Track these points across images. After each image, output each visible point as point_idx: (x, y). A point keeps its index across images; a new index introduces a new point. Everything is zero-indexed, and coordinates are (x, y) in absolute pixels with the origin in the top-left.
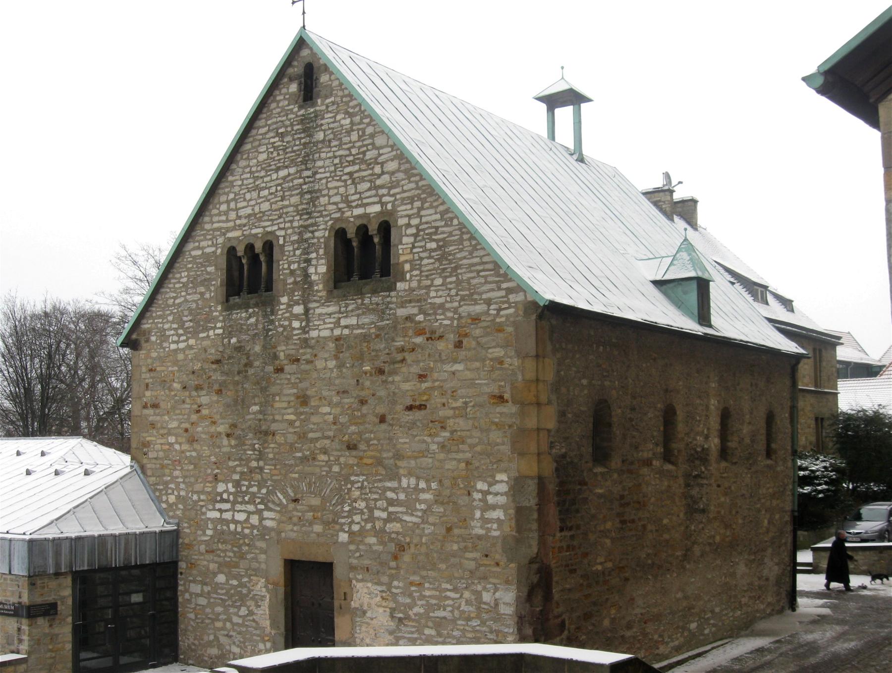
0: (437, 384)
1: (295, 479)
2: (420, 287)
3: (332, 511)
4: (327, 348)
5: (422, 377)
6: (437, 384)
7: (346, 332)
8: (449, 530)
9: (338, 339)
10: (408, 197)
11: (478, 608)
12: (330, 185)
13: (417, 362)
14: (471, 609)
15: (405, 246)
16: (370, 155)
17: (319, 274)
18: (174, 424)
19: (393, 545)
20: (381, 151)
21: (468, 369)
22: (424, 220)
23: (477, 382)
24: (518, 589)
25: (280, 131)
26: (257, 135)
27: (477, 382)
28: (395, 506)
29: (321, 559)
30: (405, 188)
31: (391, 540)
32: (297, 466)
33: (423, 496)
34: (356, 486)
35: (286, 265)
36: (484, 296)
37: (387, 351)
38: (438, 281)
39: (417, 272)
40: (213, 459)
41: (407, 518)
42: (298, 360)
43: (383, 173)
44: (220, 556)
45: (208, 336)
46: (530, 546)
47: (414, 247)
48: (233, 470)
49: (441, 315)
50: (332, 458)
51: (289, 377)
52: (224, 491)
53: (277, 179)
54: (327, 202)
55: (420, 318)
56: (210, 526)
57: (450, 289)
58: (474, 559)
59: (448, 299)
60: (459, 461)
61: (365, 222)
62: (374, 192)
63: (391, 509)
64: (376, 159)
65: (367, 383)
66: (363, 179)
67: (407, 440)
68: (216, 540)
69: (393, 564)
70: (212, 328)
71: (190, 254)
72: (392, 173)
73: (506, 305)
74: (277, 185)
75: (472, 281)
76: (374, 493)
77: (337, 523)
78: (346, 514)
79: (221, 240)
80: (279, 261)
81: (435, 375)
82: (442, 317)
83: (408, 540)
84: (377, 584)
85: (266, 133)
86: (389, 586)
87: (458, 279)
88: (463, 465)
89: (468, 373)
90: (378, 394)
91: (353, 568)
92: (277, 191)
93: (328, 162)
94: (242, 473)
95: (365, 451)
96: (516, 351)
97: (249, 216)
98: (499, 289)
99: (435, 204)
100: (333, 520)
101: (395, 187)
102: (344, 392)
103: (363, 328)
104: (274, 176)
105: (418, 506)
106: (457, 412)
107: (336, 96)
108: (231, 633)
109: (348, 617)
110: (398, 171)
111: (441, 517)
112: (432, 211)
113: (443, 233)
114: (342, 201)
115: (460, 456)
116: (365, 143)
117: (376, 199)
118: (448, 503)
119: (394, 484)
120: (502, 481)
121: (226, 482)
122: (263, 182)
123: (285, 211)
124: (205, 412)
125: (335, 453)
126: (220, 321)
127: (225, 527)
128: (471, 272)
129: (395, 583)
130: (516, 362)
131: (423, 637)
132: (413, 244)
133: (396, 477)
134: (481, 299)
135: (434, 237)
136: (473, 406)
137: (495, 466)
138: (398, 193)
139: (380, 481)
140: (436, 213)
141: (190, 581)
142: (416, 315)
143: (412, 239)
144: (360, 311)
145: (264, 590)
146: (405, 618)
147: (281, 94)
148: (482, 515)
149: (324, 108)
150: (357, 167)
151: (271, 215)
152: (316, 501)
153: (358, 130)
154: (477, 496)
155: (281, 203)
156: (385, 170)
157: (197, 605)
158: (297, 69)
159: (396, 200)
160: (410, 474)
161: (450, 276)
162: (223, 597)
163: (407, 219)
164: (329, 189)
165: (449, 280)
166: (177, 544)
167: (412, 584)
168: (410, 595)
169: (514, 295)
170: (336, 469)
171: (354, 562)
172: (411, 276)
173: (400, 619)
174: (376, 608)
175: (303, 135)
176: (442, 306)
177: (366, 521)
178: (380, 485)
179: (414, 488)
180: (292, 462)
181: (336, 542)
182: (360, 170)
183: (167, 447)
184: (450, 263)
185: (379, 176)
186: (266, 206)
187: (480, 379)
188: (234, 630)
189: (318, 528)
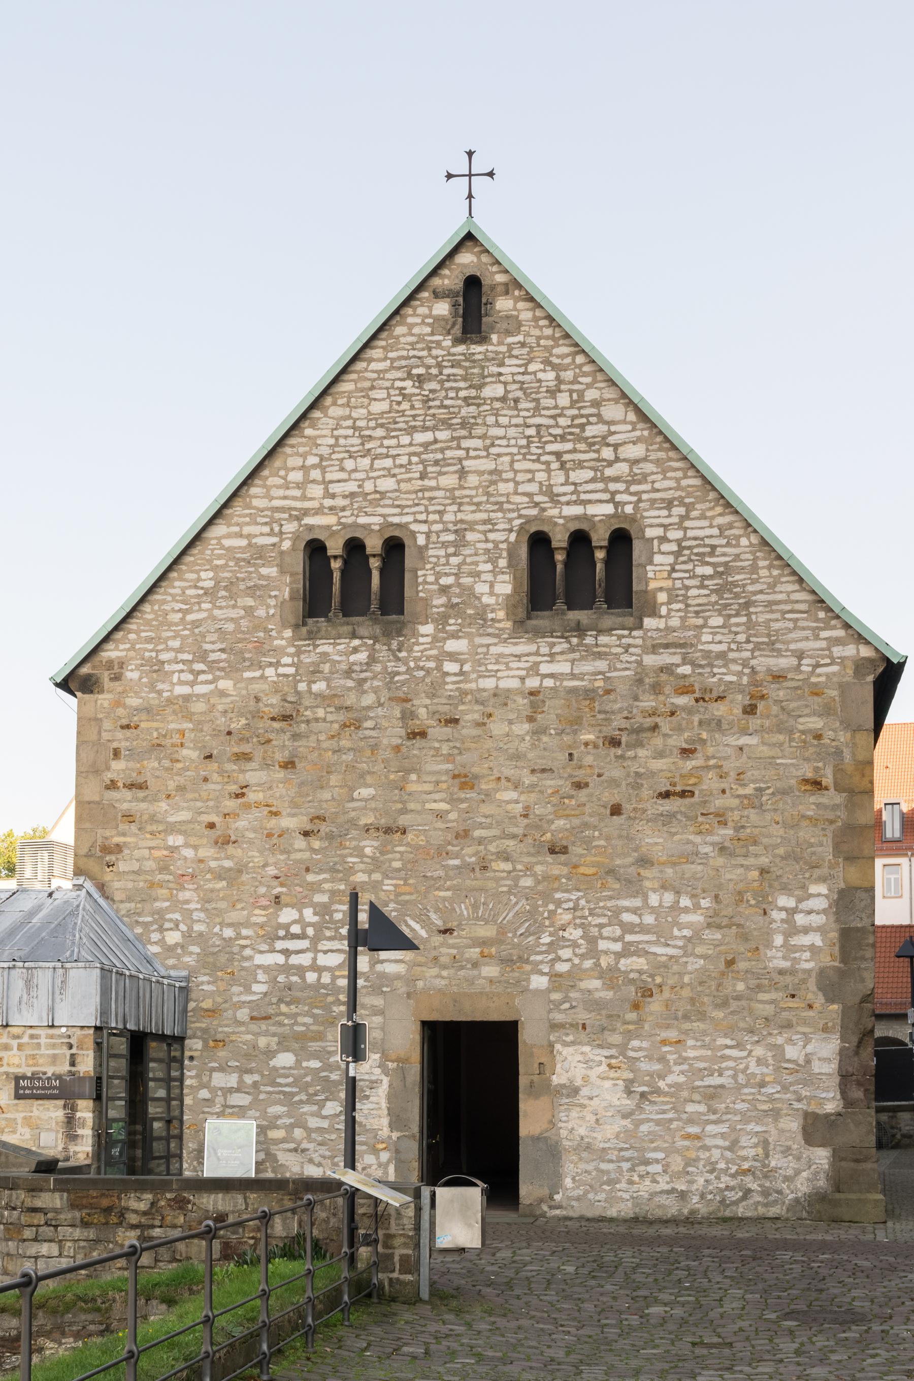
0: (712, 762)
1: (444, 899)
2: (684, 627)
3: (519, 945)
4: (511, 705)
5: (687, 752)
6: (712, 762)
7: (549, 683)
8: (730, 963)
10: (663, 500)
11: (777, 1069)
12: (517, 466)
13: (679, 729)
14: (765, 1070)
15: (658, 568)
16: (590, 431)
17: (497, 596)
20: (613, 428)
21: (764, 743)
22: (690, 534)
23: (778, 761)
24: (843, 1039)
25: (415, 371)
26: (366, 370)
27: (778, 761)
28: (636, 933)
29: (494, 1016)
30: (657, 485)
32: (451, 879)
33: (685, 918)
34: (565, 906)
36: (792, 646)
37: (625, 714)
39: (681, 606)
40: (271, 871)
43: (617, 459)
44: (281, 1024)
45: (262, 677)
46: (863, 980)
47: (673, 570)
48: (315, 888)
49: (720, 667)
51: (437, 745)
52: (295, 922)
53: (411, 444)
55: (686, 670)
56: (261, 977)
57: (736, 633)
58: (772, 1002)
59: (734, 646)
60: (747, 868)
61: (584, 526)
62: (600, 486)
63: (629, 938)
64: (604, 438)
65: (589, 760)
67: (661, 840)
68: (274, 1000)
69: (632, 1016)
71: (219, 543)
72: (635, 462)
73: (828, 661)
74: (410, 454)
75: (772, 624)
76: (599, 916)
77: (527, 961)
78: (544, 948)
79: (290, 527)
80: (415, 571)
81: (710, 750)
82: (724, 670)
83: (658, 980)
84: (600, 1046)
85: (385, 371)
86: (623, 1049)
87: (750, 620)
88: (755, 874)
89: (765, 748)
90: (607, 774)
91: (555, 1026)
92: (410, 463)
93: (512, 432)
95: (581, 856)
96: (842, 722)
97: (352, 495)
98: (817, 638)
99: (709, 514)
100: (520, 958)
101: (640, 483)
102: (543, 771)
103: (582, 680)
104: (405, 440)
105: (676, 932)
106: (746, 802)
107: (528, 334)
108: (305, 1145)
109: (544, 1102)
110: (645, 459)
111: (716, 946)
113: (724, 555)
114: (541, 492)
115: (751, 861)
116: (583, 412)
117: (606, 496)
118: (729, 926)
119: (637, 902)
120: (819, 895)
121: (299, 906)
122: (382, 446)
123: (427, 494)
124: (252, 796)
125: (526, 859)
127: (295, 979)
128: (772, 612)
129: (635, 1043)
130: (843, 737)
131: (684, 1116)
134: (787, 650)
135: (707, 559)
136: (773, 794)
137: (807, 875)
139: (611, 898)
140: (711, 526)
141: (213, 1070)
142: (678, 666)
144: (577, 655)
145: (378, 1071)
146: (652, 1093)
147: (415, 315)
148: (786, 941)
149: (503, 349)
150: (569, 446)
152: (487, 932)
153: (571, 392)
154: (777, 915)
155: (420, 482)
156: (622, 456)
158: (451, 280)
159: (640, 500)
160: (664, 887)
161: (737, 615)
162: (287, 1089)
163: (662, 529)
164: (516, 472)
165: (734, 620)
166: (185, 1011)
167: (664, 1042)
168: (662, 1059)
169: (840, 648)
170: (527, 882)
171: (559, 1017)
172: (669, 610)
173: (643, 1095)
174: (599, 1082)
175: (462, 384)
176: (722, 655)
177: (583, 957)
180: (441, 873)
181: (526, 990)
182: (575, 451)
183: (165, 853)
184: (737, 596)
185: (610, 464)
186: (387, 484)
188: (310, 1140)
189: (490, 971)
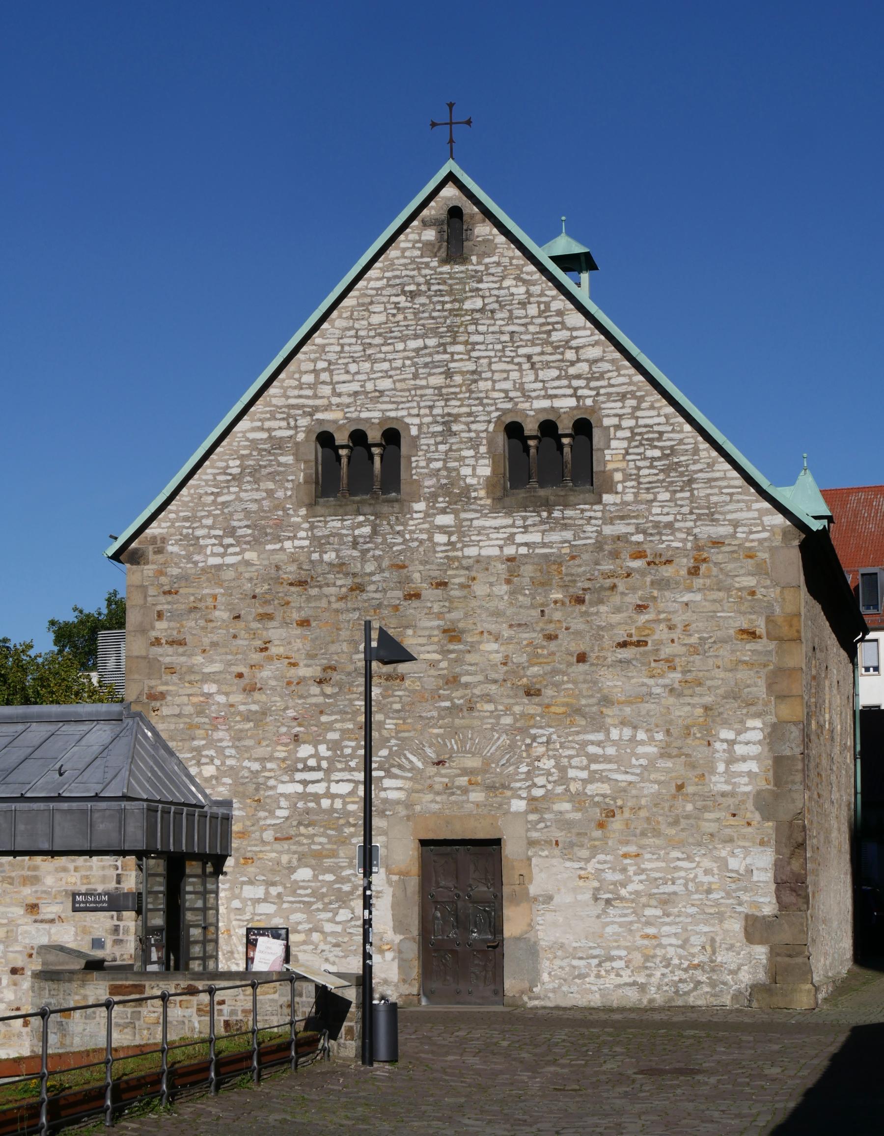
0: (662, 616)
6: (662, 616)
7: (523, 550)
8: (680, 787)
9: (511, 559)
10: (618, 393)
12: (494, 367)
13: (634, 589)
15: (614, 452)
17: (479, 477)
18: (216, 667)
19: (598, 810)
20: (575, 334)
22: (641, 422)
24: (777, 852)
25: (407, 288)
28: (600, 762)
30: (612, 382)
31: (597, 804)
32: (443, 718)
35: (421, 464)
36: (729, 517)
38: (664, 496)
39: (633, 483)
40: (291, 713)
41: (620, 777)
42: (445, 584)
43: (579, 360)
50: (501, 707)
52: (311, 756)
53: (405, 350)
54: (490, 388)
55: (639, 538)
56: (283, 803)
59: (679, 517)
63: (594, 767)
64: (567, 342)
66: (547, 365)
67: (620, 683)
69: (598, 833)
70: (289, 538)
73: (760, 528)
76: (568, 748)
78: (523, 776)
79: (303, 422)
81: (661, 606)
88: (699, 711)
89: (706, 604)
91: (532, 843)
92: (404, 366)
93: (490, 338)
94: (343, 731)
97: (356, 394)
101: (598, 379)
102: (519, 625)
103: (552, 547)
104: (400, 346)
112: (653, 413)
115: (696, 700)
117: (570, 391)
119: (600, 736)
123: (419, 392)
124: (274, 650)
125: (507, 701)
126: (303, 530)
132: (627, 450)
133: (601, 727)
134: (725, 520)
135: (656, 443)
138: (602, 387)
139: (578, 733)
140: (659, 415)
142: (632, 534)
143: (625, 444)
144: (547, 527)
150: (538, 349)
151: (394, 396)
152: (472, 763)
153: (539, 303)
155: (413, 382)
157: (254, 914)
160: (623, 723)
161: (682, 491)
162: (306, 899)
164: (493, 372)
165: (679, 495)
169: (770, 517)
170: (507, 720)
171: (535, 835)
172: (624, 487)
173: (608, 902)
178: (577, 738)
179: (629, 740)
180: (435, 714)
181: (507, 812)
182: (542, 353)
184: (682, 474)
185: (573, 363)
187: (723, 611)
189: (477, 796)
